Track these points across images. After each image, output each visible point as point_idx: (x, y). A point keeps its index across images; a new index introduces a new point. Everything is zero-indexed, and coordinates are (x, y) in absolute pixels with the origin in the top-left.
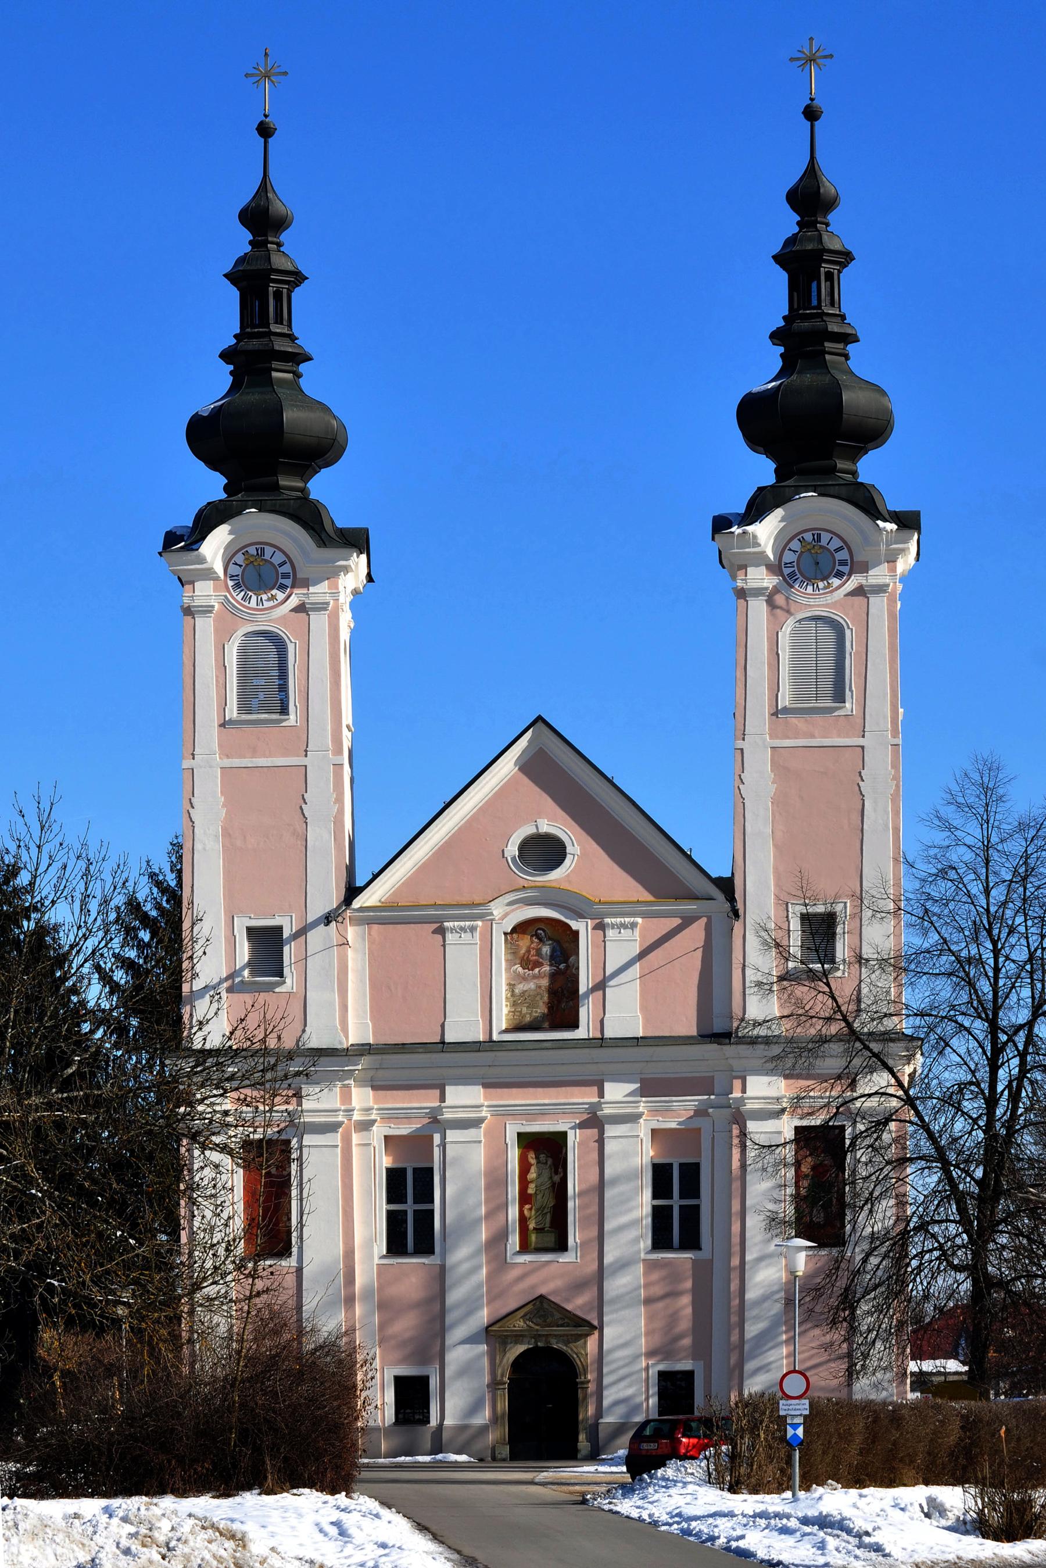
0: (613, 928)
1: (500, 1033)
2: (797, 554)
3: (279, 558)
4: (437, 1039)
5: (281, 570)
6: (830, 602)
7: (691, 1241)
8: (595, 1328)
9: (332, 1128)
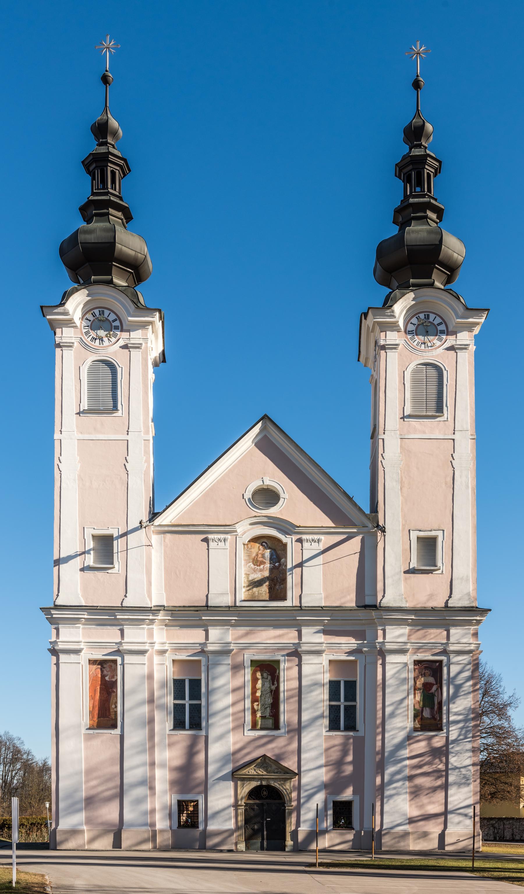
0: (307, 542)
1: (241, 601)
2: (416, 326)
3: (112, 317)
4: (204, 604)
5: (114, 324)
6: (434, 354)
7: (351, 726)
8: (296, 774)
9: (142, 653)
